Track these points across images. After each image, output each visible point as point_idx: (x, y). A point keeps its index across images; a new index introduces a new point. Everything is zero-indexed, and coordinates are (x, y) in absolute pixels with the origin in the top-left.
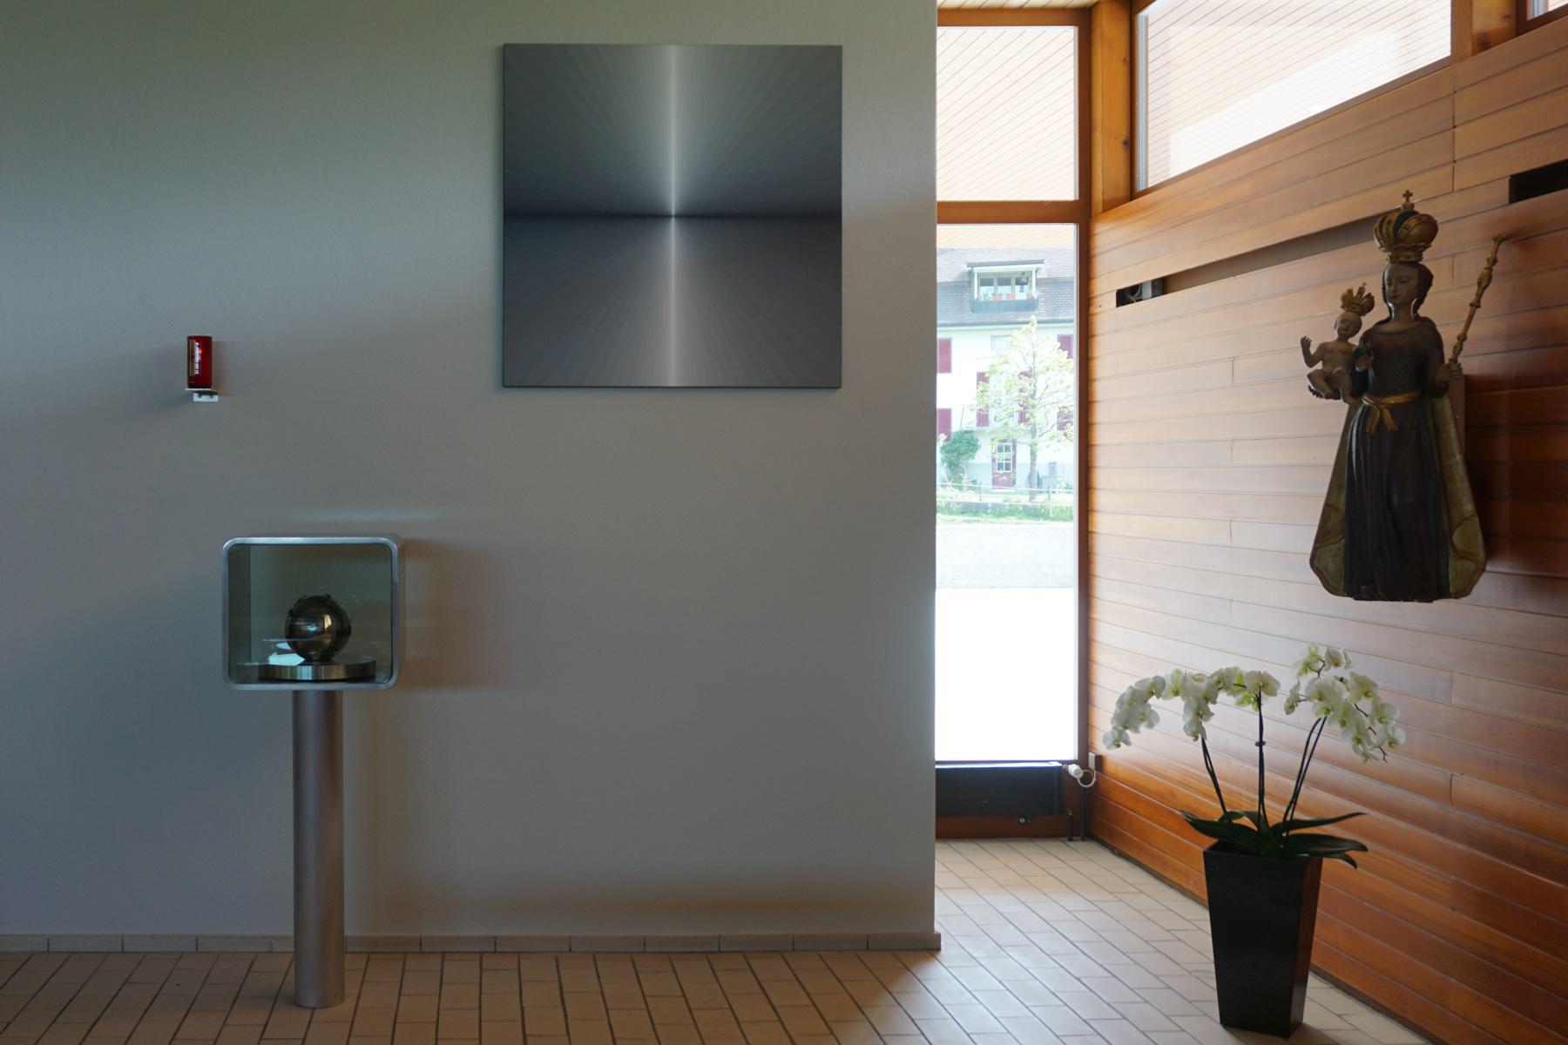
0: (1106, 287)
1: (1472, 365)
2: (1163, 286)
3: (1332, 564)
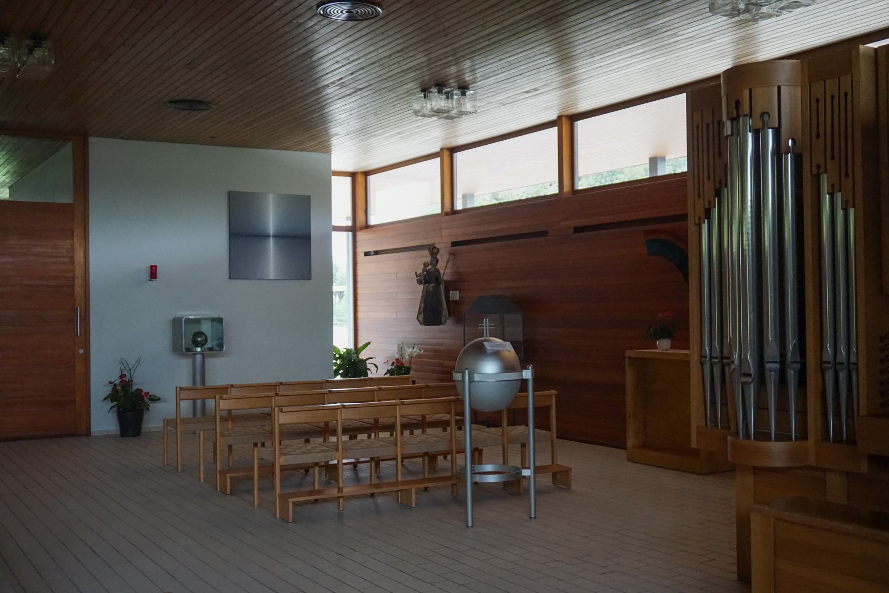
0: (361, 250)
1: (445, 278)
2: (377, 253)
3: (421, 319)
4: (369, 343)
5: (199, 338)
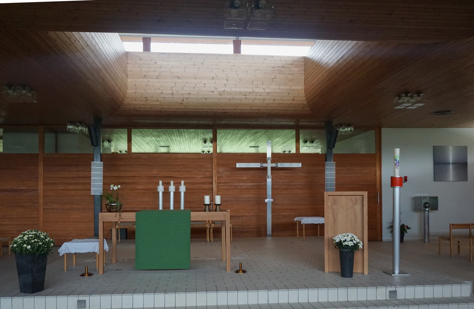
5: (427, 204)
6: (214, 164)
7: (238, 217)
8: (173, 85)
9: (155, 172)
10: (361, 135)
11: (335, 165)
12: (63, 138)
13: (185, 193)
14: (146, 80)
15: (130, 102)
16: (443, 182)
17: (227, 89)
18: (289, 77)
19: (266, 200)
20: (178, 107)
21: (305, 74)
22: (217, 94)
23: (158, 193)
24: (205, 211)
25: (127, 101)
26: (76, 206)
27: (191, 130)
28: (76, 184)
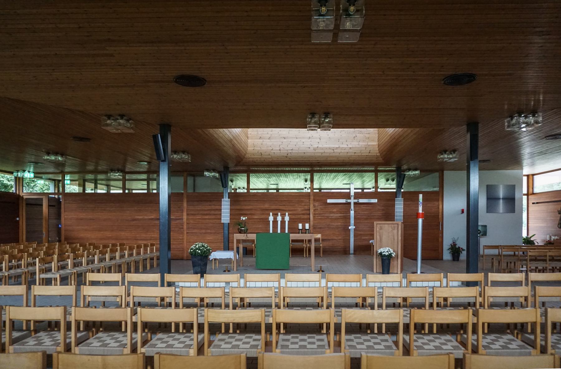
0: (531, 202)
2: (537, 203)
3: (559, 226)
4: (535, 235)
6: (311, 200)
7: (329, 240)
8: (280, 143)
9: (267, 206)
10: (429, 176)
11: (403, 201)
12: (199, 180)
13: (289, 222)
14: (261, 140)
15: (250, 156)
16: (494, 214)
17: (320, 146)
18: (366, 136)
19: (350, 228)
20: (283, 159)
21: (378, 133)
22: (313, 149)
23: (269, 221)
24: (299, 233)
25: (247, 156)
26: (209, 231)
27: (294, 174)
28: (210, 215)
